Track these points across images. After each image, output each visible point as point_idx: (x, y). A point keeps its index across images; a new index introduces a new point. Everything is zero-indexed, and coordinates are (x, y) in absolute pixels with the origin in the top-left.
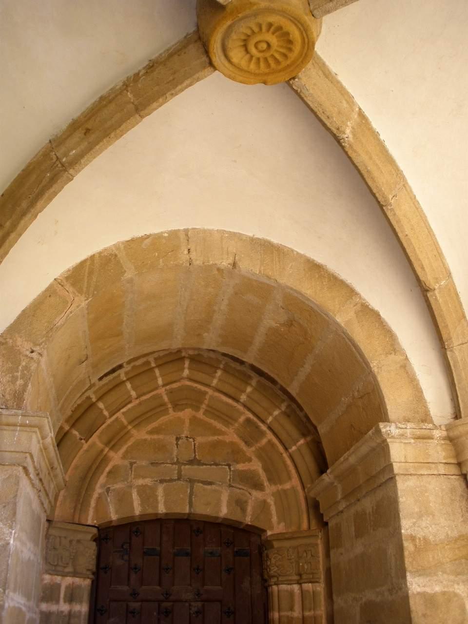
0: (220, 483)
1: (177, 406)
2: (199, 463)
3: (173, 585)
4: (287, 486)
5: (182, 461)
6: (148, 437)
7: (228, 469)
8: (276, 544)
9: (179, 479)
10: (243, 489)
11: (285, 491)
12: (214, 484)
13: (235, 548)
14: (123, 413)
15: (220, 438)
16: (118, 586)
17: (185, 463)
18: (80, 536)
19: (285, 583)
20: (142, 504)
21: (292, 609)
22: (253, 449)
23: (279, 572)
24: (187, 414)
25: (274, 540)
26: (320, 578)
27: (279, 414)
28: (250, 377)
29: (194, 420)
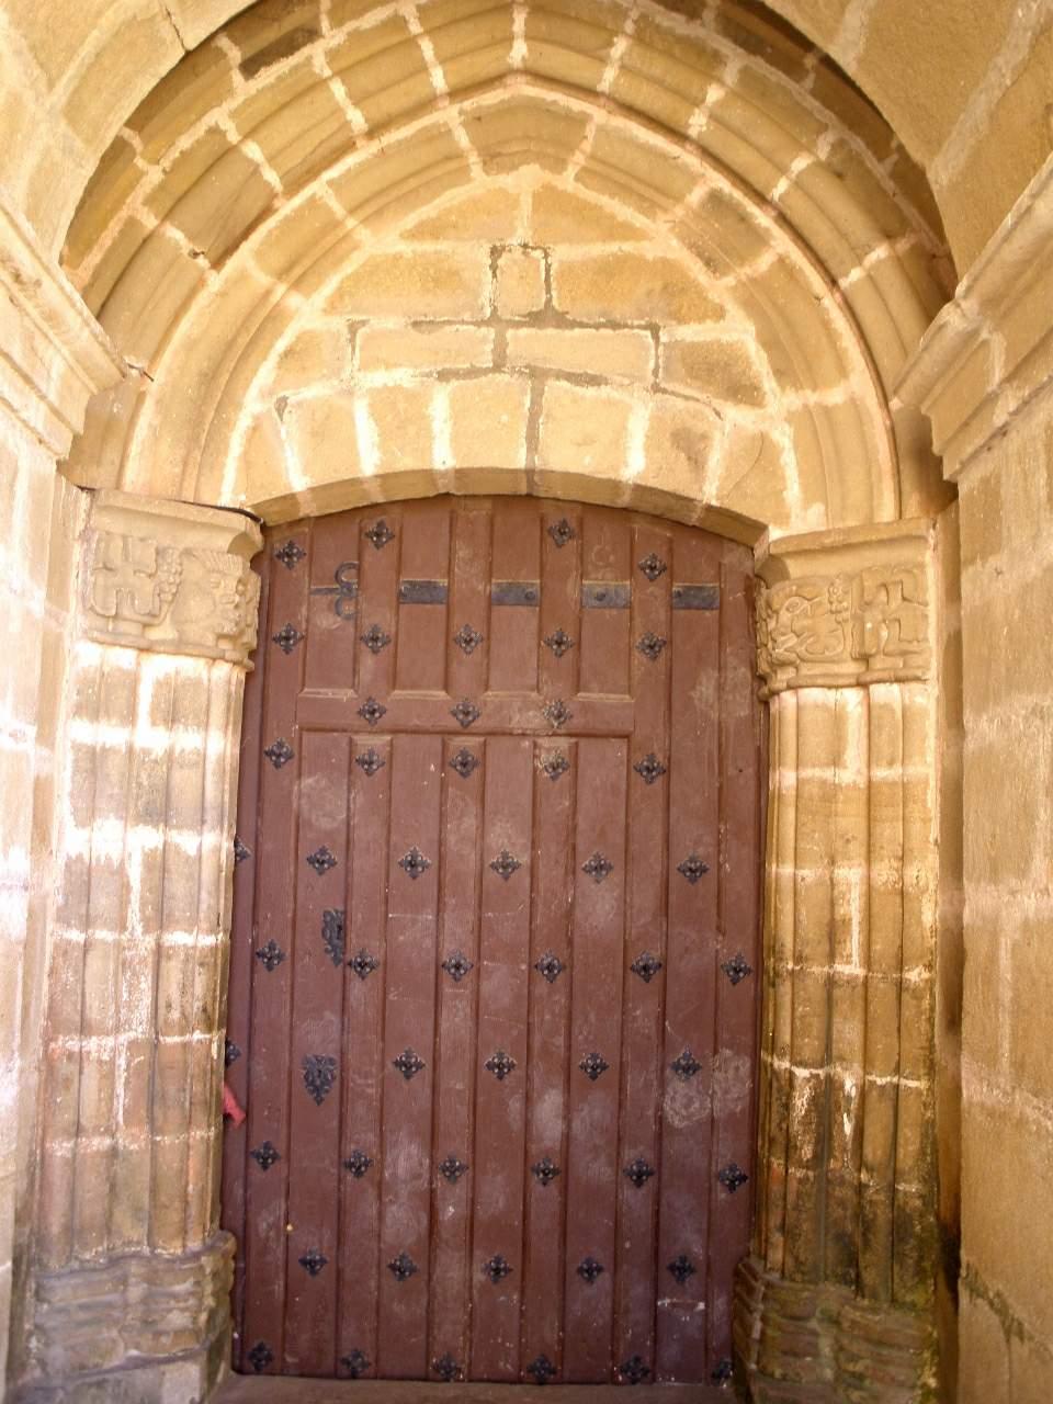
0: (626, 381)
1: (493, 158)
2: (562, 321)
3: (487, 688)
4: (835, 396)
5: (508, 317)
6: (406, 248)
7: (651, 341)
8: (795, 568)
9: (497, 367)
10: (698, 400)
11: (827, 411)
12: (606, 384)
13: (675, 584)
14: (331, 183)
15: (628, 247)
16: (322, 690)
17: (519, 322)
18: (193, 539)
19: (820, 681)
20: (385, 437)
21: (836, 760)
22: (730, 280)
23: (801, 650)
24: (526, 179)
25: (789, 554)
26: (926, 668)
27: (809, 167)
28: (717, 59)
29: (547, 199)
